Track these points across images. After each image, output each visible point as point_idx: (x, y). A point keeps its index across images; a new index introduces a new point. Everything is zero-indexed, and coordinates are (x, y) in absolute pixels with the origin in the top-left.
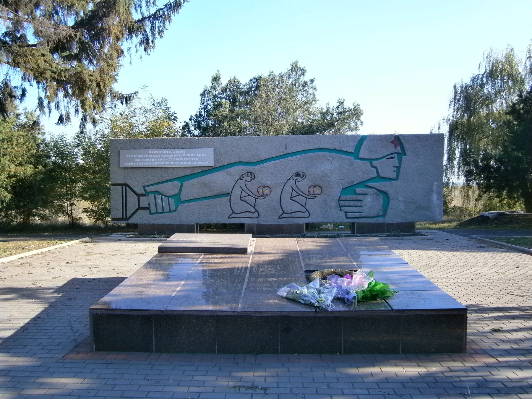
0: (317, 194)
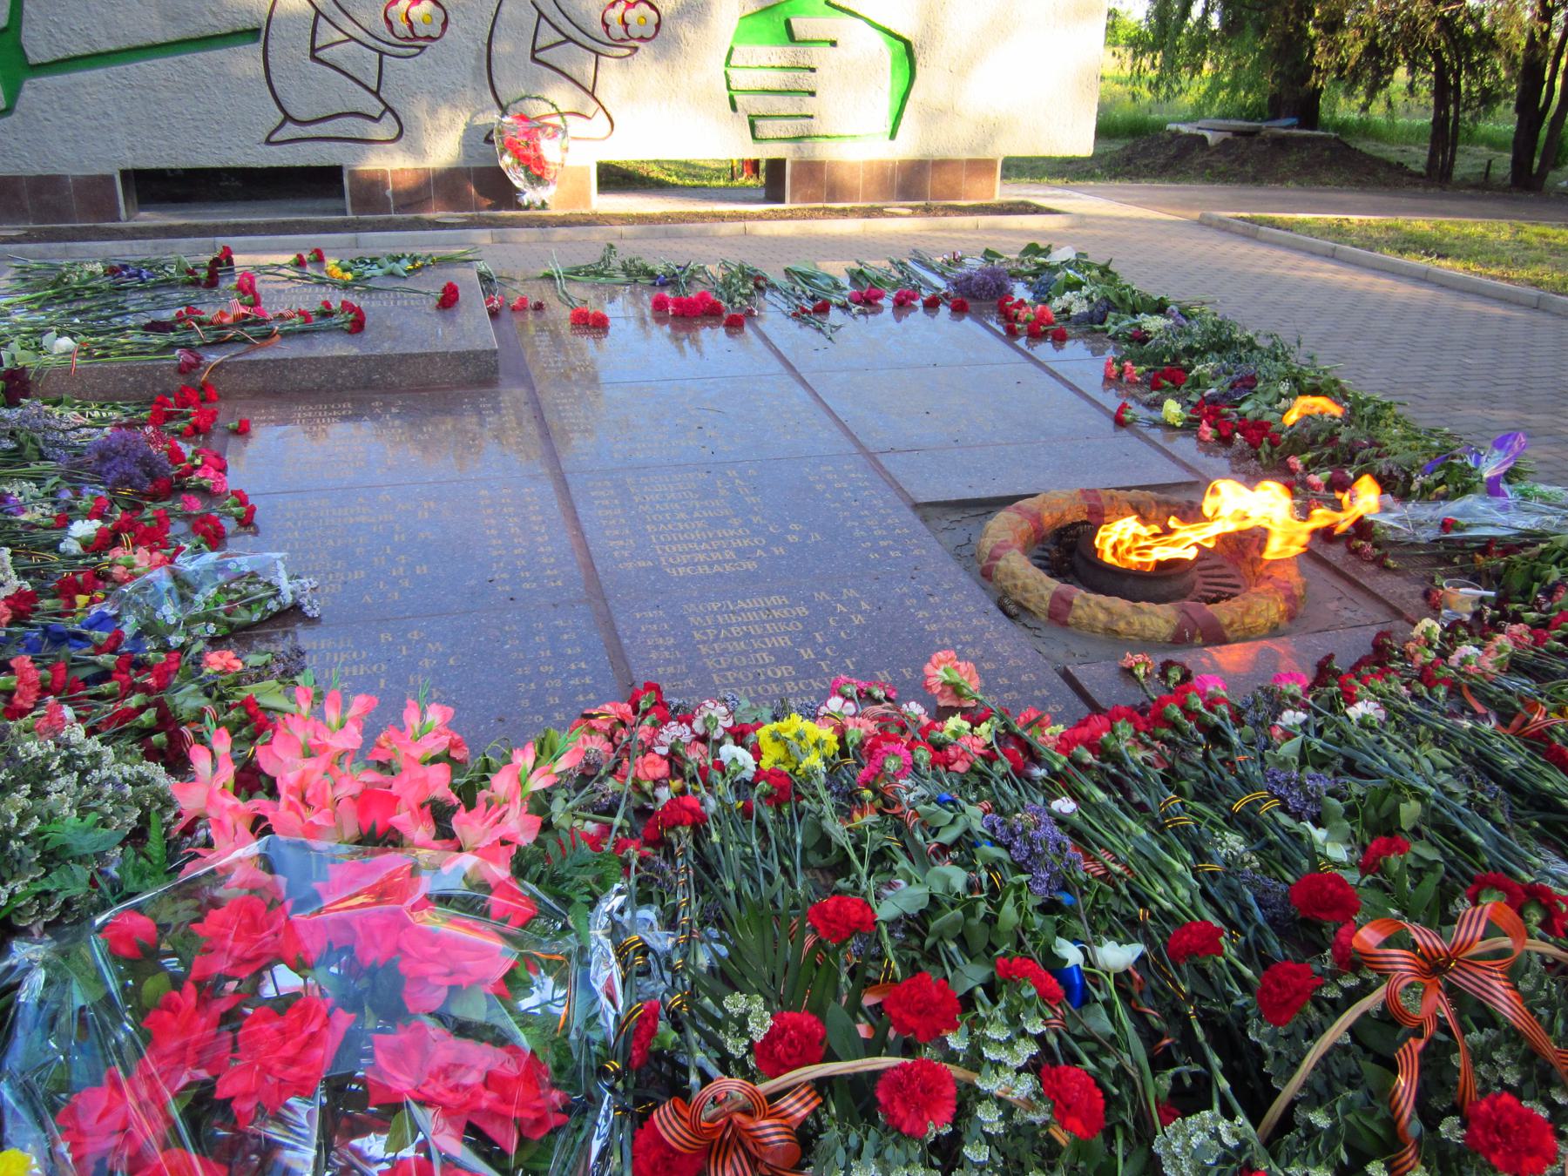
0: (429, 38)
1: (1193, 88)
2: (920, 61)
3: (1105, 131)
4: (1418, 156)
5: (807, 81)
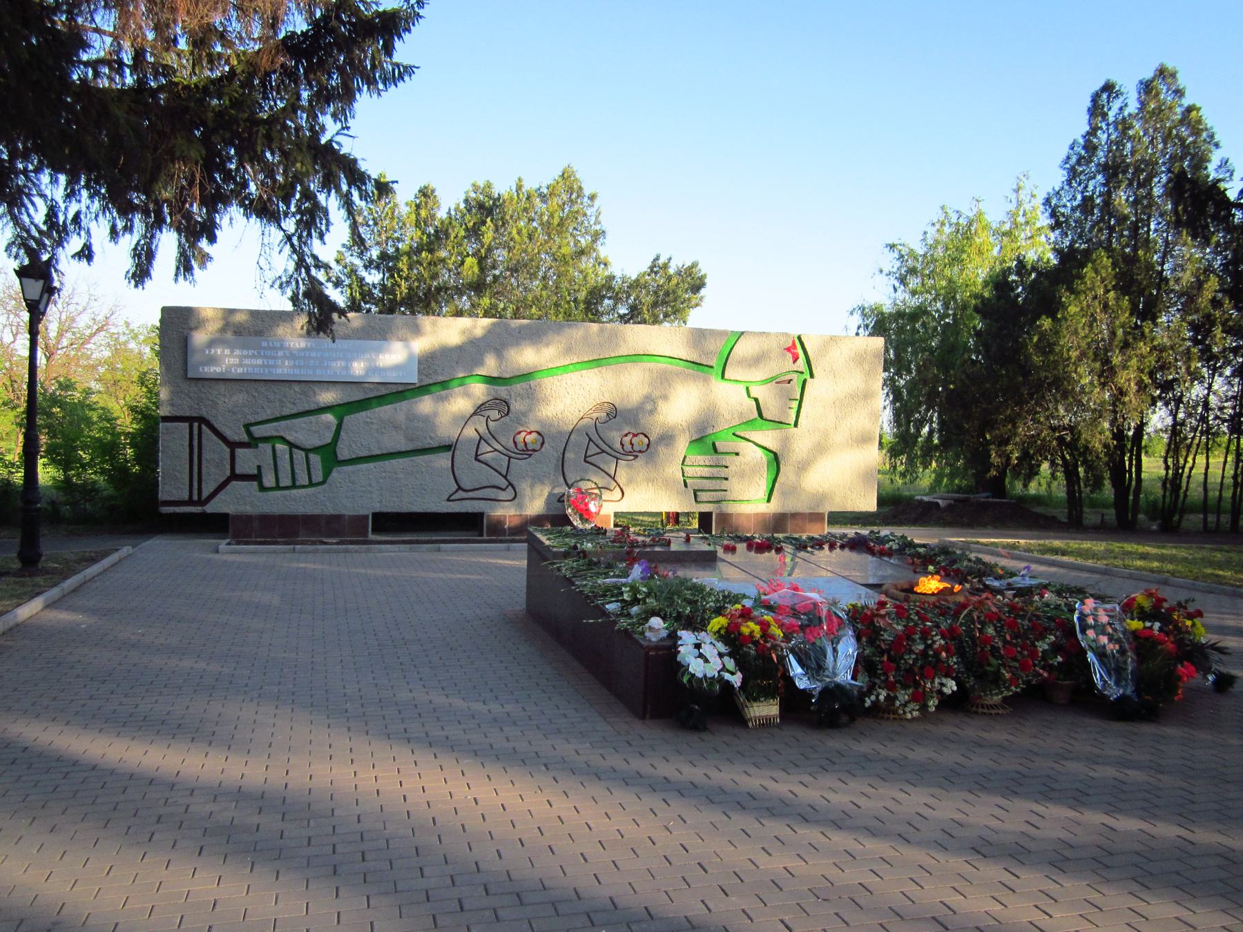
0: (534, 450)
1: (926, 478)
2: (782, 463)
3: (881, 501)
4: (1062, 514)
5: (723, 472)
